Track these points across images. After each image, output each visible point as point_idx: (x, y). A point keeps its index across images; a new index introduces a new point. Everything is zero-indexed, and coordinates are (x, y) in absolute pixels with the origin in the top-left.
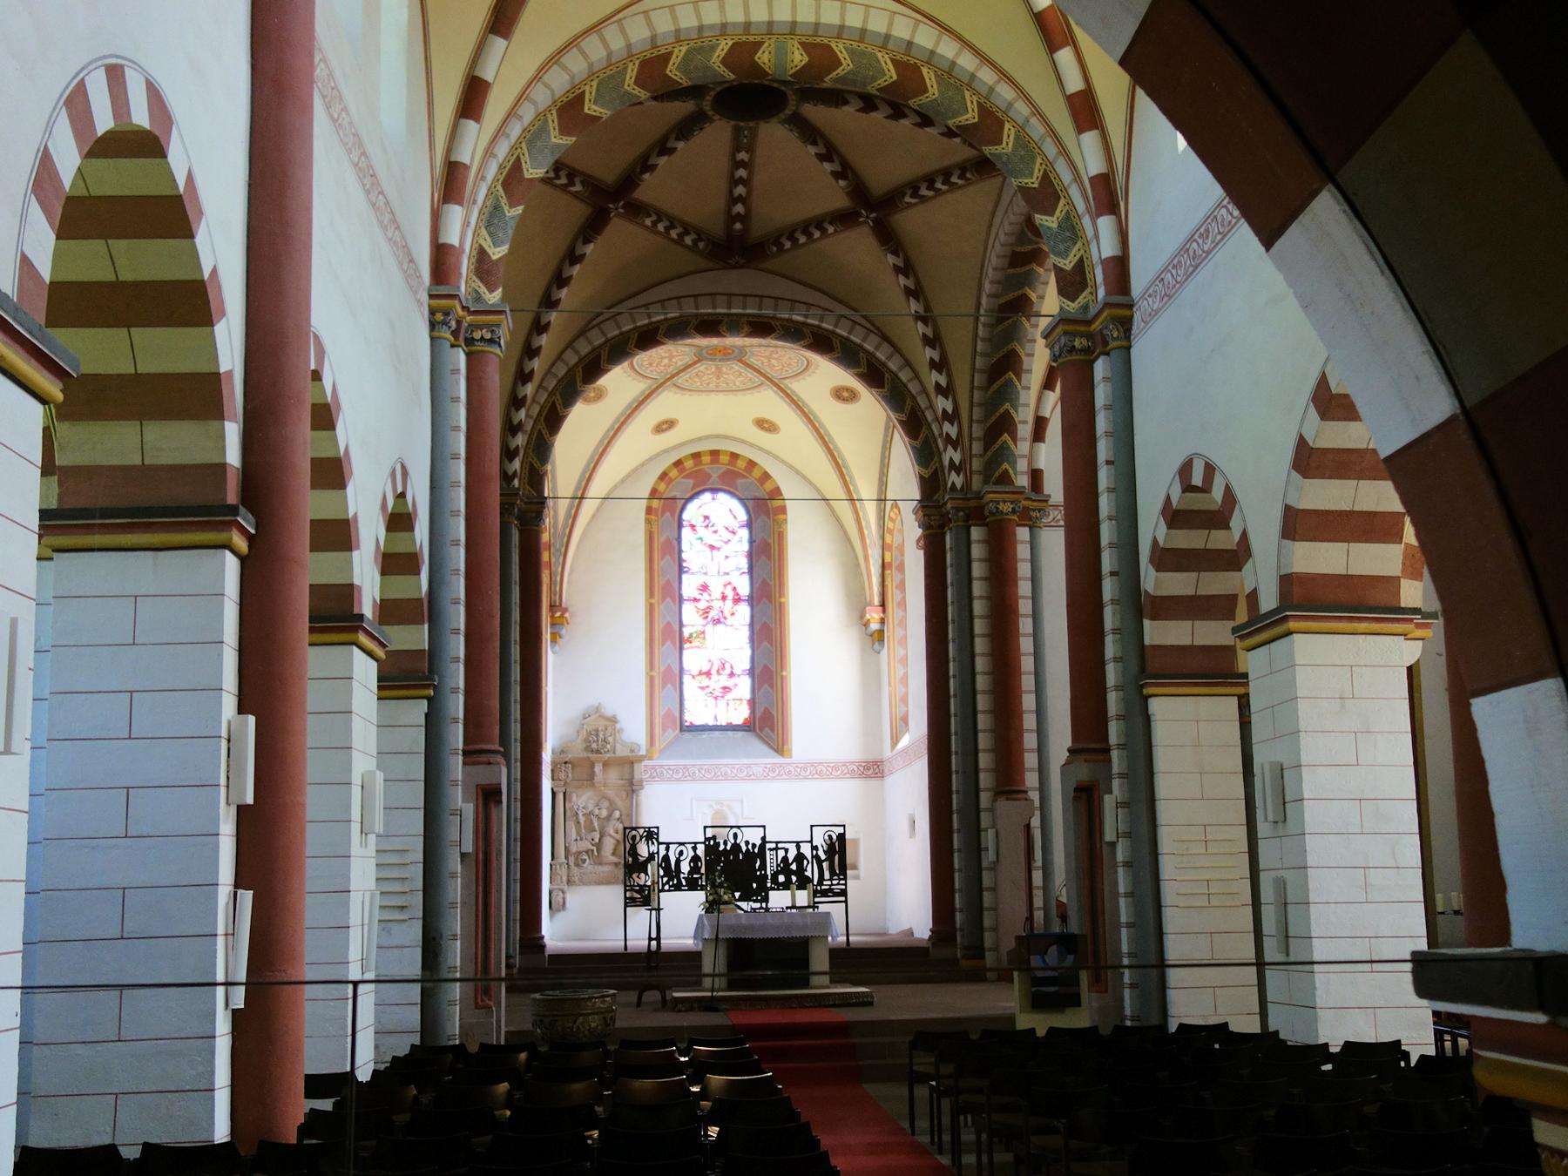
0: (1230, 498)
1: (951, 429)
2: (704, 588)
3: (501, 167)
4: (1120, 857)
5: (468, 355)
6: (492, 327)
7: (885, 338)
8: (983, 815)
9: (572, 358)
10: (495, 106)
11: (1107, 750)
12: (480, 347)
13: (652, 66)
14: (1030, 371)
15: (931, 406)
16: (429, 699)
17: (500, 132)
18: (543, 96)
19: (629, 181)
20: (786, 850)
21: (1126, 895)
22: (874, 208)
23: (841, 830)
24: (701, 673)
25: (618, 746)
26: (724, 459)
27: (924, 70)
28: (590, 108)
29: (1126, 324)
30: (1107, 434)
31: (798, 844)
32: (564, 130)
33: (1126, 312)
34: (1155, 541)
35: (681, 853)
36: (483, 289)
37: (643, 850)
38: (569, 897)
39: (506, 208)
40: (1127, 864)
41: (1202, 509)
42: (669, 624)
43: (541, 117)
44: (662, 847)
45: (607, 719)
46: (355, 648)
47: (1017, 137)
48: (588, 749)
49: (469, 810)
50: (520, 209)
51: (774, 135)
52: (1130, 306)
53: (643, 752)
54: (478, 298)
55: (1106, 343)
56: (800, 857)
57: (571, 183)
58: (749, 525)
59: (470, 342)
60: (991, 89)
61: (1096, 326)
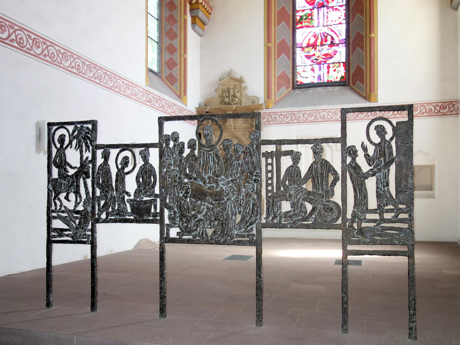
20: (296, 157)
23: (403, 117)
24: (308, 46)
25: (243, 99)
31: (317, 144)
35: (126, 162)
37: (73, 157)
44: (99, 153)
45: (236, 80)
48: (223, 102)
56: (321, 169)
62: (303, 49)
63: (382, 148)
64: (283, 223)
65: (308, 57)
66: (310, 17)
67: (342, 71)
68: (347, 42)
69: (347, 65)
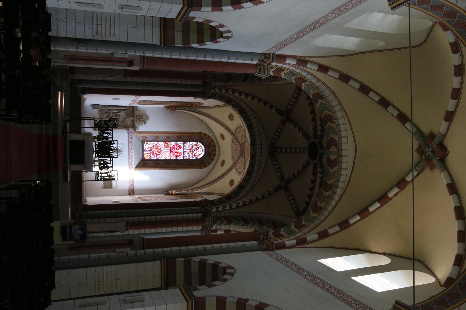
0: (225, 280)
1: (227, 208)
2: (180, 147)
3: (305, 77)
4: (111, 254)
5: (256, 64)
6: (264, 71)
7: (251, 189)
8: (121, 218)
9: (245, 106)
10: (320, 75)
11: (144, 249)
12: (259, 68)
13: (330, 118)
14: (243, 228)
15: (234, 202)
16: (161, 45)
17: (314, 76)
18: (323, 88)
19: (291, 121)
20: (110, 164)
21: (99, 256)
22: (285, 185)
26: (214, 153)
27: (330, 192)
28: (320, 102)
29: (267, 249)
30: (237, 245)
31: (112, 167)
32: (314, 94)
33: (271, 249)
34: (208, 260)
36: (274, 70)
38: (97, 110)
39: (294, 77)
40: (108, 256)
41: (218, 273)
42: (171, 138)
43: (317, 88)
45: (146, 121)
46: (182, 6)
47: (314, 217)
48: (137, 116)
49: (126, 56)
50: (294, 82)
51: (305, 158)
52: (272, 250)
53: (136, 130)
54: (272, 68)
55: (262, 244)
57: (291, 105)
58: (196, 159)
59: (260, 65)
60: (327, 210)
61: (266, 241)
62: (156, 144)
63: (111, 176)
64: (87, 130)
65: (153, 146)
66: (167, 146)
67: (147, 158)
68: (157, 160)
69: (150, 160)
